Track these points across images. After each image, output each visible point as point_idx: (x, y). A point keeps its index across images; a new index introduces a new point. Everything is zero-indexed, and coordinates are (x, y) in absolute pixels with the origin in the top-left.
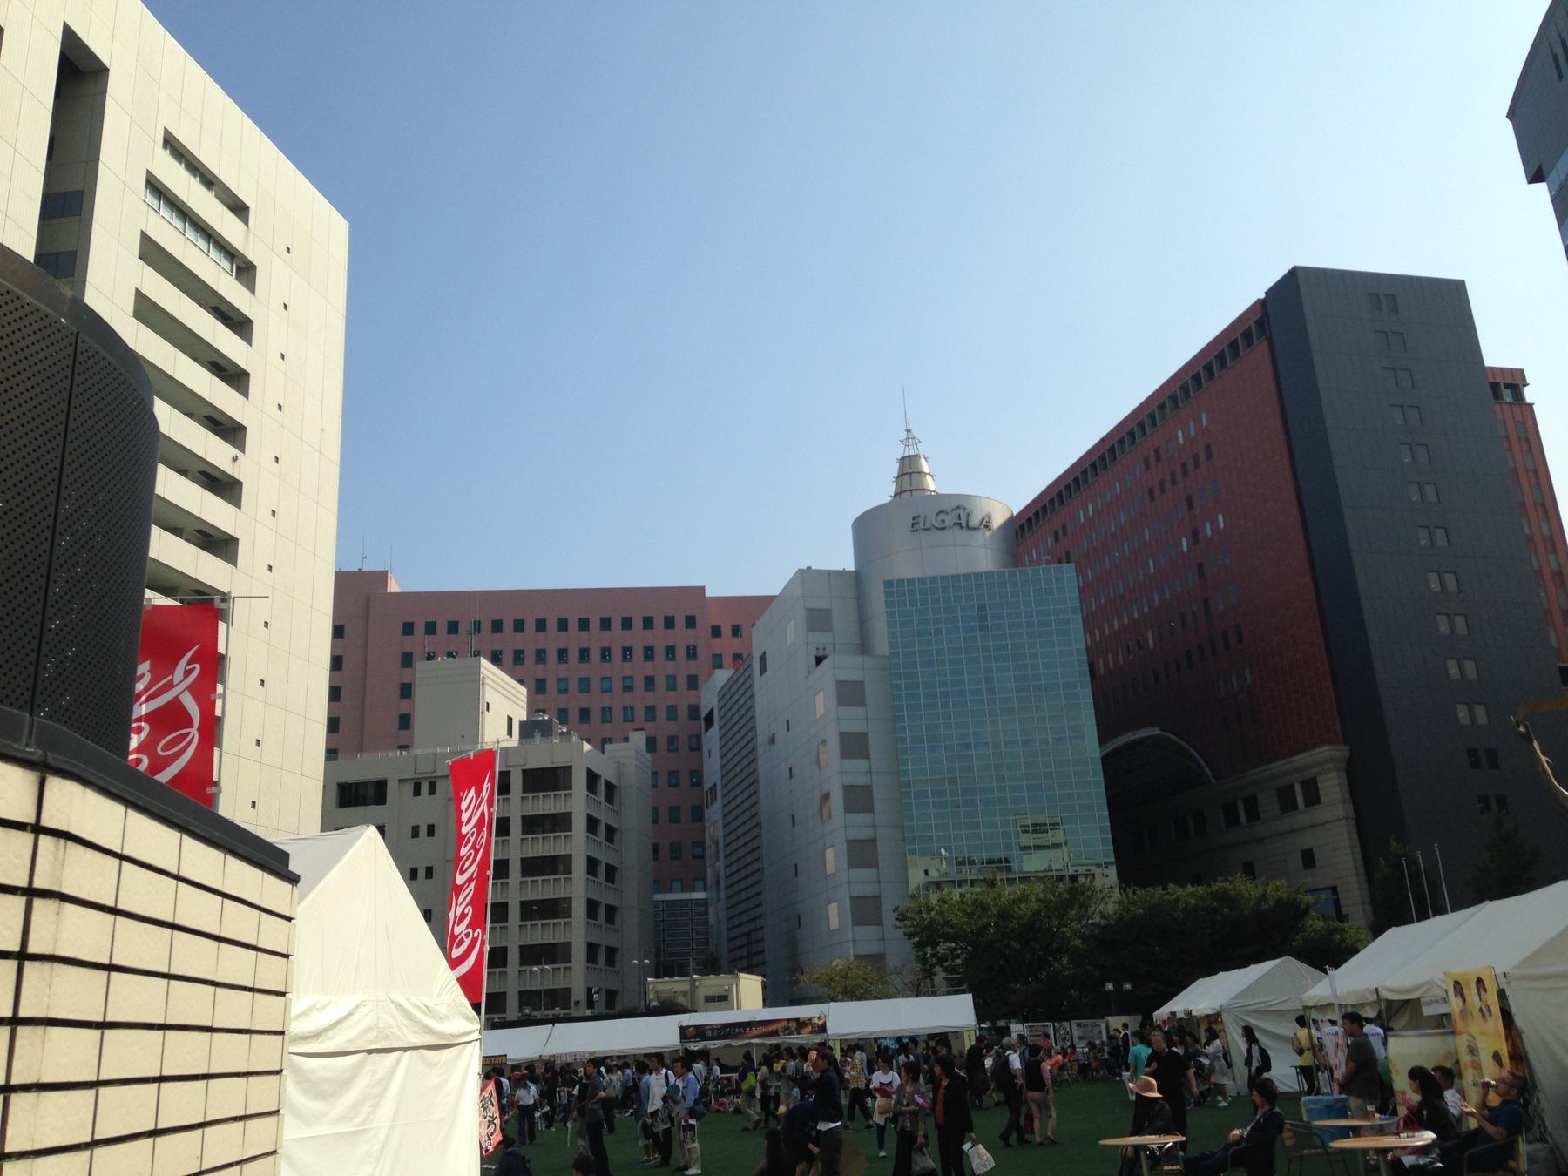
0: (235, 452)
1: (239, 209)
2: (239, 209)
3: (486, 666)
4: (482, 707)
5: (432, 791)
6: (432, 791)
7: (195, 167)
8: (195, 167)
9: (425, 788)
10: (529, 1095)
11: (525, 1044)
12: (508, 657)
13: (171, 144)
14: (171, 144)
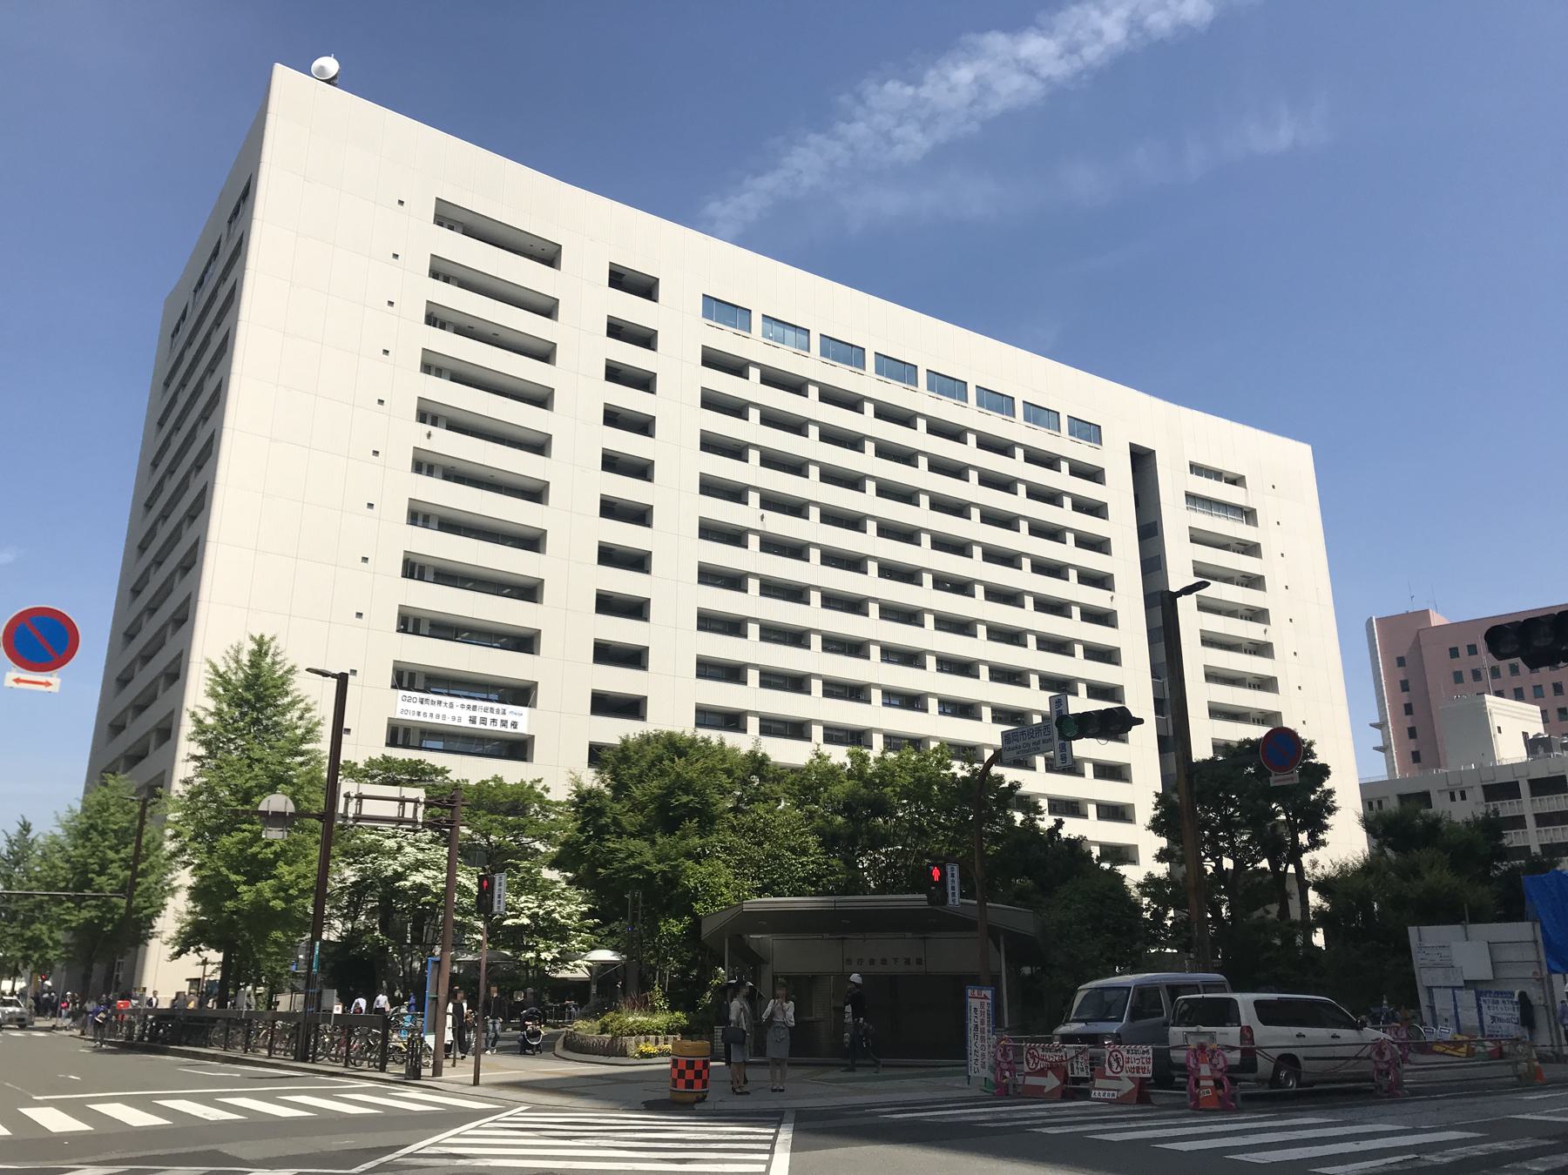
0: (1263, 626)
1: (1237, 481)
2: (1237, 481)
3: (1491, 700)
4: (1494, 731)
5: (1463, 797)
6: (1463, 797)
7: (1216, 475)
8: (1216, 475)
9: (1458, 796)
10: (471, 1036)
11: (483, 967)
12: (1528, 691)
13: (1196, 469)
14: (1196, 469)
